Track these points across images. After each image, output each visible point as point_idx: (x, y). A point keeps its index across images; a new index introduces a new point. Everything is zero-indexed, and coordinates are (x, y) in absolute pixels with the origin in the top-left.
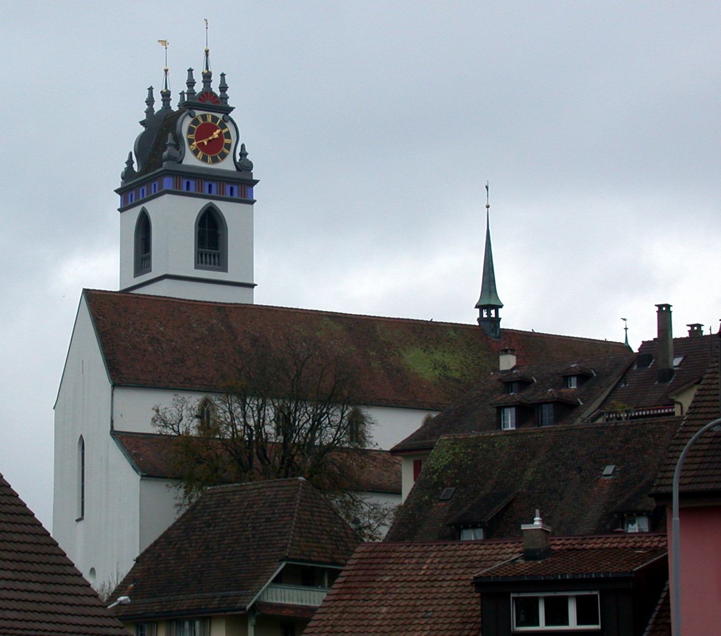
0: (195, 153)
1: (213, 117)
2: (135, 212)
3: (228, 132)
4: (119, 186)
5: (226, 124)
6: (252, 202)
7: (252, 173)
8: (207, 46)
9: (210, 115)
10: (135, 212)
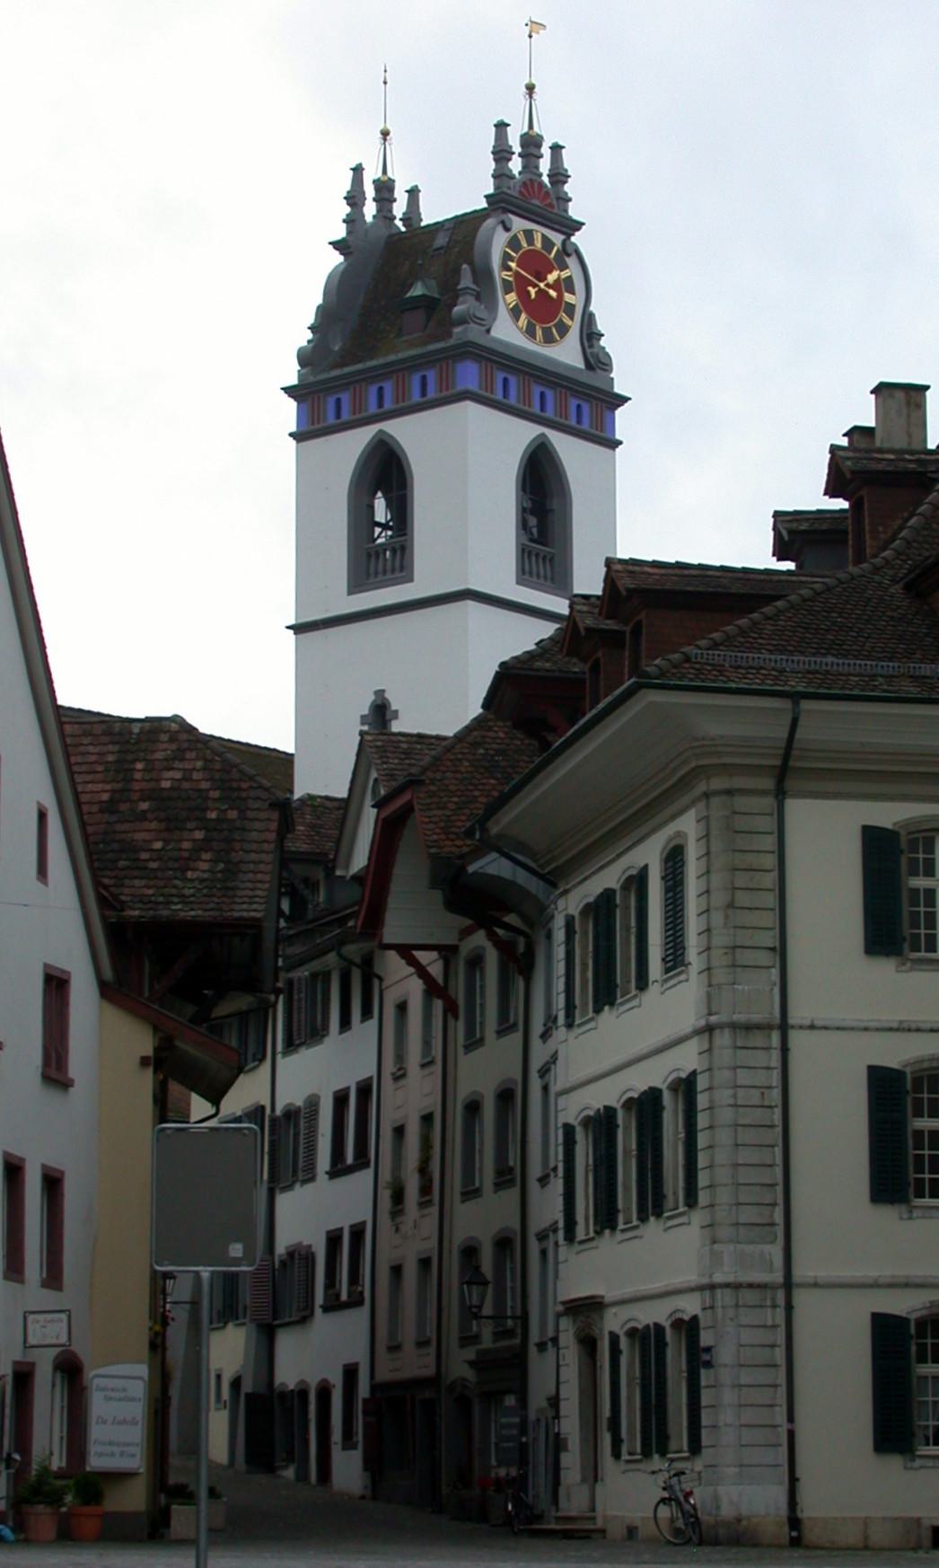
0: (515, 313)
1: (545, 238)
2: (354, 443)
3: (569, 279)
4: (293, 380)
5: (567, 259)
6: (614, 444)
7: (612, 379)
8: (530, 76)
9: (540, 231)
10: (354, 443)
